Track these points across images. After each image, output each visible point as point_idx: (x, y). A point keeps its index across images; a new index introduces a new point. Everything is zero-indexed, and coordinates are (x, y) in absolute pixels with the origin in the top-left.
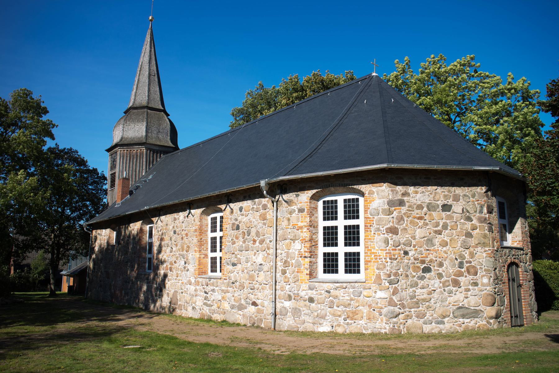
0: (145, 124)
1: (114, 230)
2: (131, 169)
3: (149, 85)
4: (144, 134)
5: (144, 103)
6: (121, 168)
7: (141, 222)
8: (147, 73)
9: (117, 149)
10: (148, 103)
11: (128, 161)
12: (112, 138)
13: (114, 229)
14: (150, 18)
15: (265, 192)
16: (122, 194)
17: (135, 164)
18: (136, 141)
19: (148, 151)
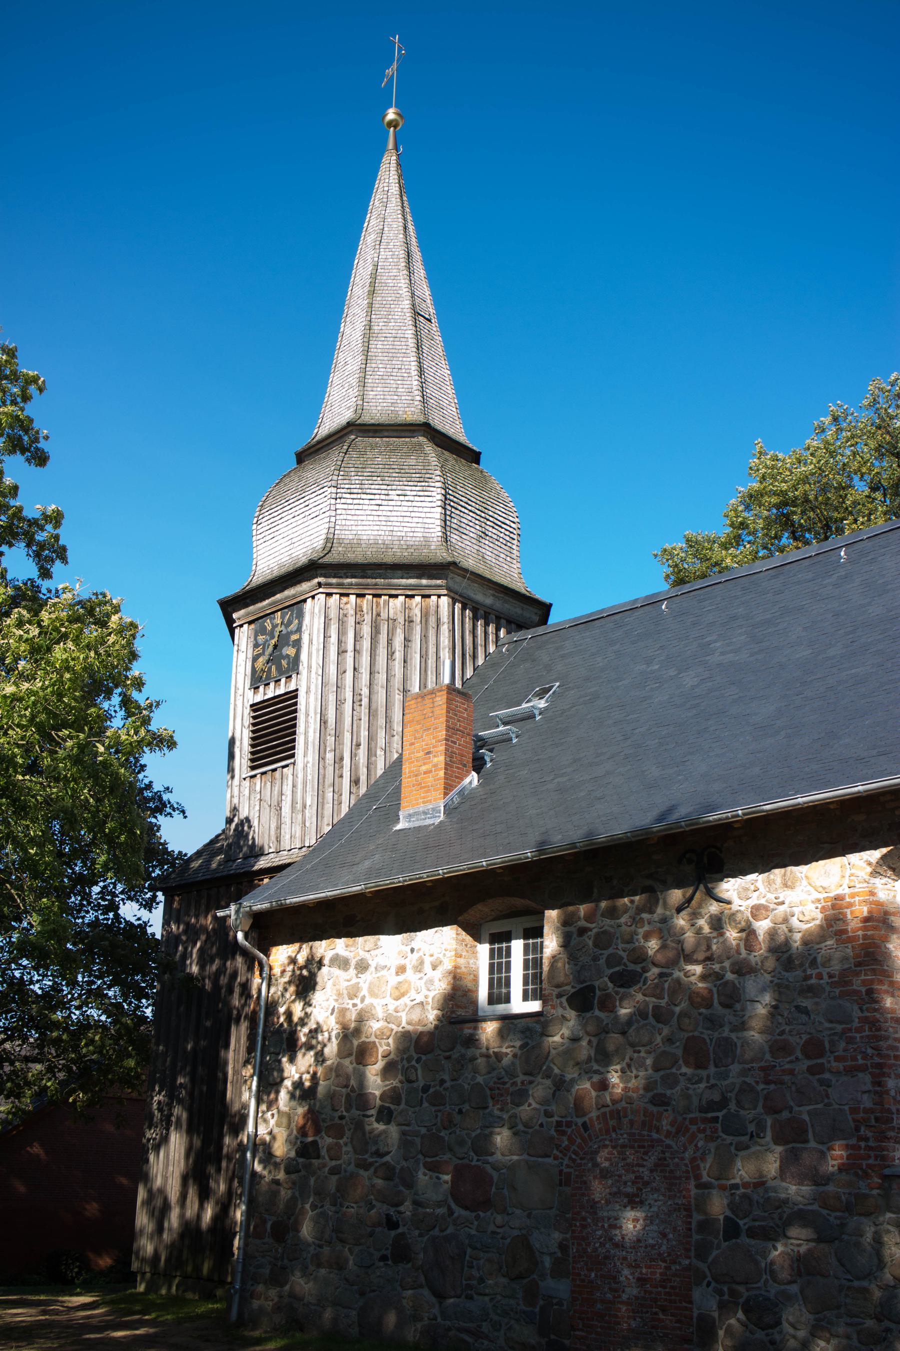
0: (437, 495)
1: (478, 939)
2: (381, 678)
3: (419, 347)
4: (436, 531)
5: (410, 412)
6: (332, 669)
7: (875, 855)
8: (406, 304)
9: (305, 586)
10: (424, 411)
11: (366, 644)
12: (245, 551)
13: (475, 932)
14: (391, 115)
15: (240, 936)
16: (447, 766)
17: (399, 655)
18: (405, 556)
19: (458, 606)
